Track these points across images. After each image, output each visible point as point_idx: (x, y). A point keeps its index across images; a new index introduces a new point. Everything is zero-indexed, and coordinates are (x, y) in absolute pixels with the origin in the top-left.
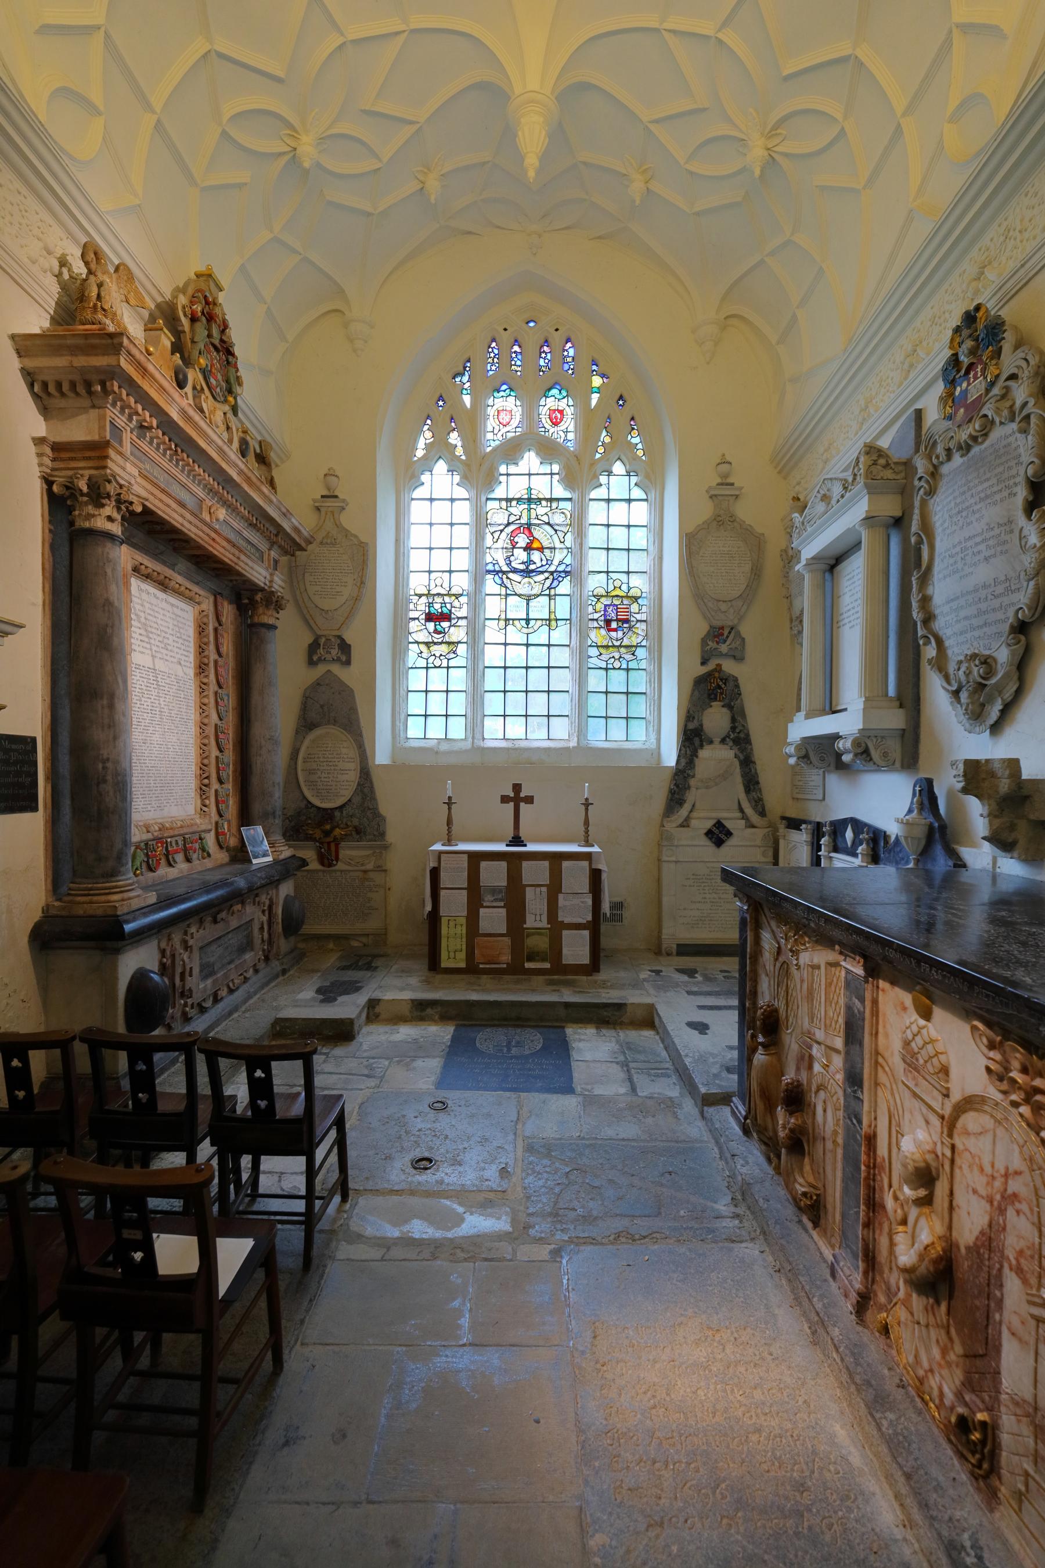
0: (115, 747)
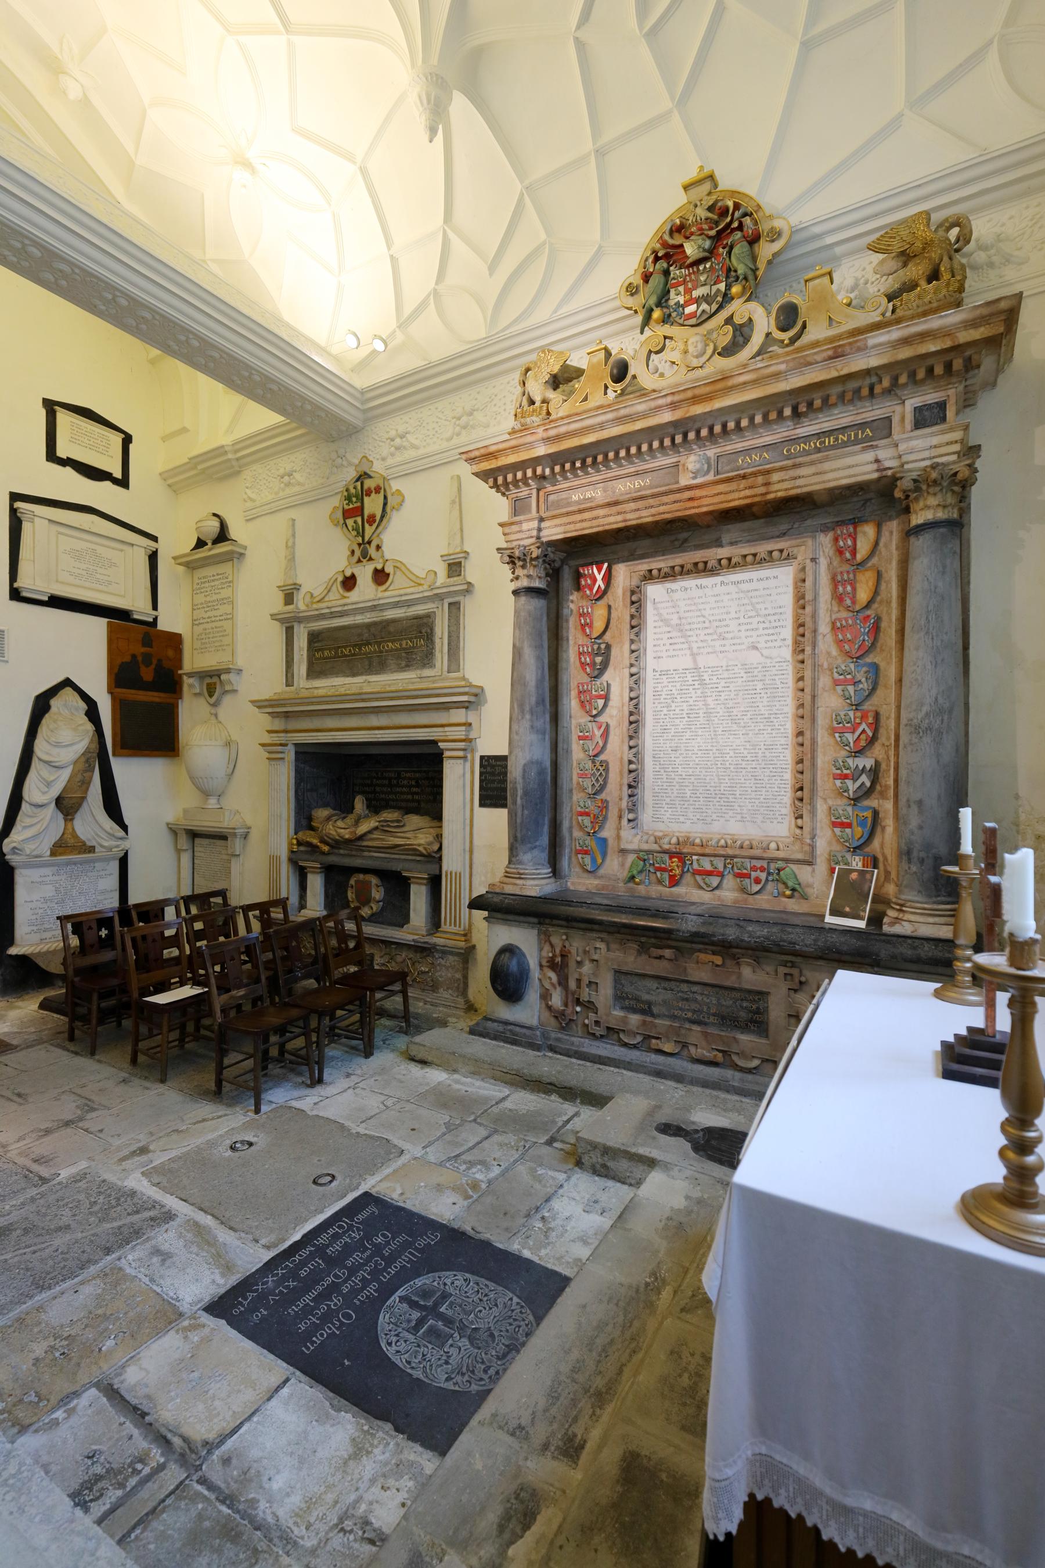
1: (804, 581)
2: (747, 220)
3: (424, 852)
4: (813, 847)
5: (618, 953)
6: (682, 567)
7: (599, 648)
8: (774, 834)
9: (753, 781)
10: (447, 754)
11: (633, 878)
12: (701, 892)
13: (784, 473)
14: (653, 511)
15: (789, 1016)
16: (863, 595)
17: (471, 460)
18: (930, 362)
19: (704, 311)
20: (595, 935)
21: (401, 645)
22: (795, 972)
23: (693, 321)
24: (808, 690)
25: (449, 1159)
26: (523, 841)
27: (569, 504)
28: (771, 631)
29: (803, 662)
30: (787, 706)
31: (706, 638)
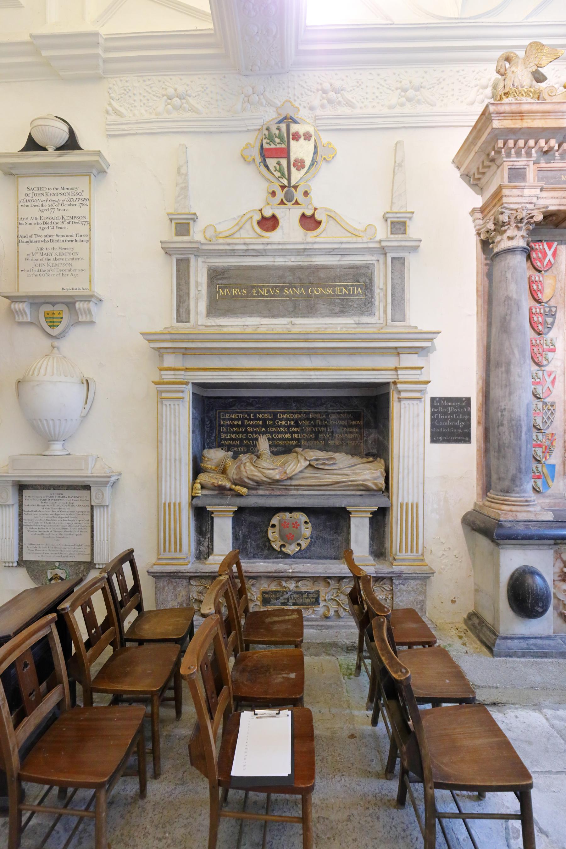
0: (510, 400)
3: (374, 487)
7: (550, 311)
21: (334, 291)
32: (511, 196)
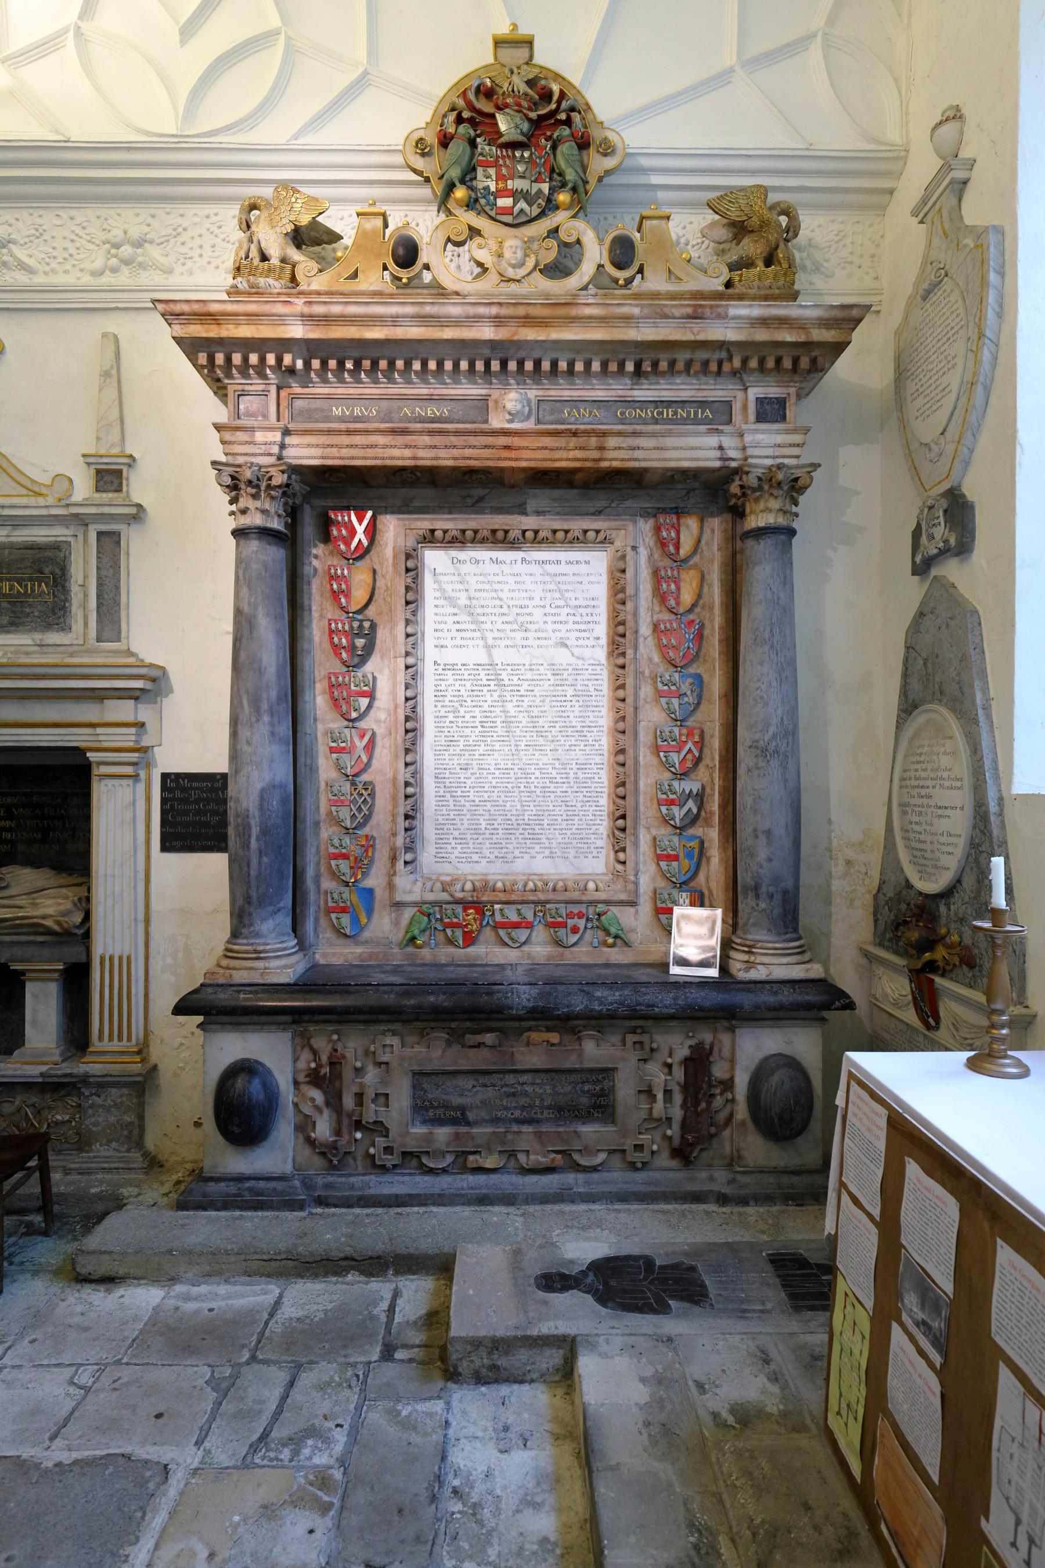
1: (624, 571)
2: (576, 117)
3: (56, 928)
4: (636, 884)
5: (417, 1049)
6: (476, 532)
7: (361, 627)
8: (589, 871)
9: (564, 808)
10: (95, 771)
11: (413, 939)
12: (506, 950)
13: (621, 439)
14: (455, 452)
15: (640, 1092)
16: (687, 597)
17: (171, 316)
18: (781, 352)
19: (522, 211)
20: (382, 1028)
22: (645, 1038)
23: (508, 219)
24: (630, 700)
25: (254, 1448)
26: (261, 902)
27: (328, 419)
28: (583, 627)
29: (623, 667)
30: (603, 718)
31: (505, 626)
32: (234, 443)
